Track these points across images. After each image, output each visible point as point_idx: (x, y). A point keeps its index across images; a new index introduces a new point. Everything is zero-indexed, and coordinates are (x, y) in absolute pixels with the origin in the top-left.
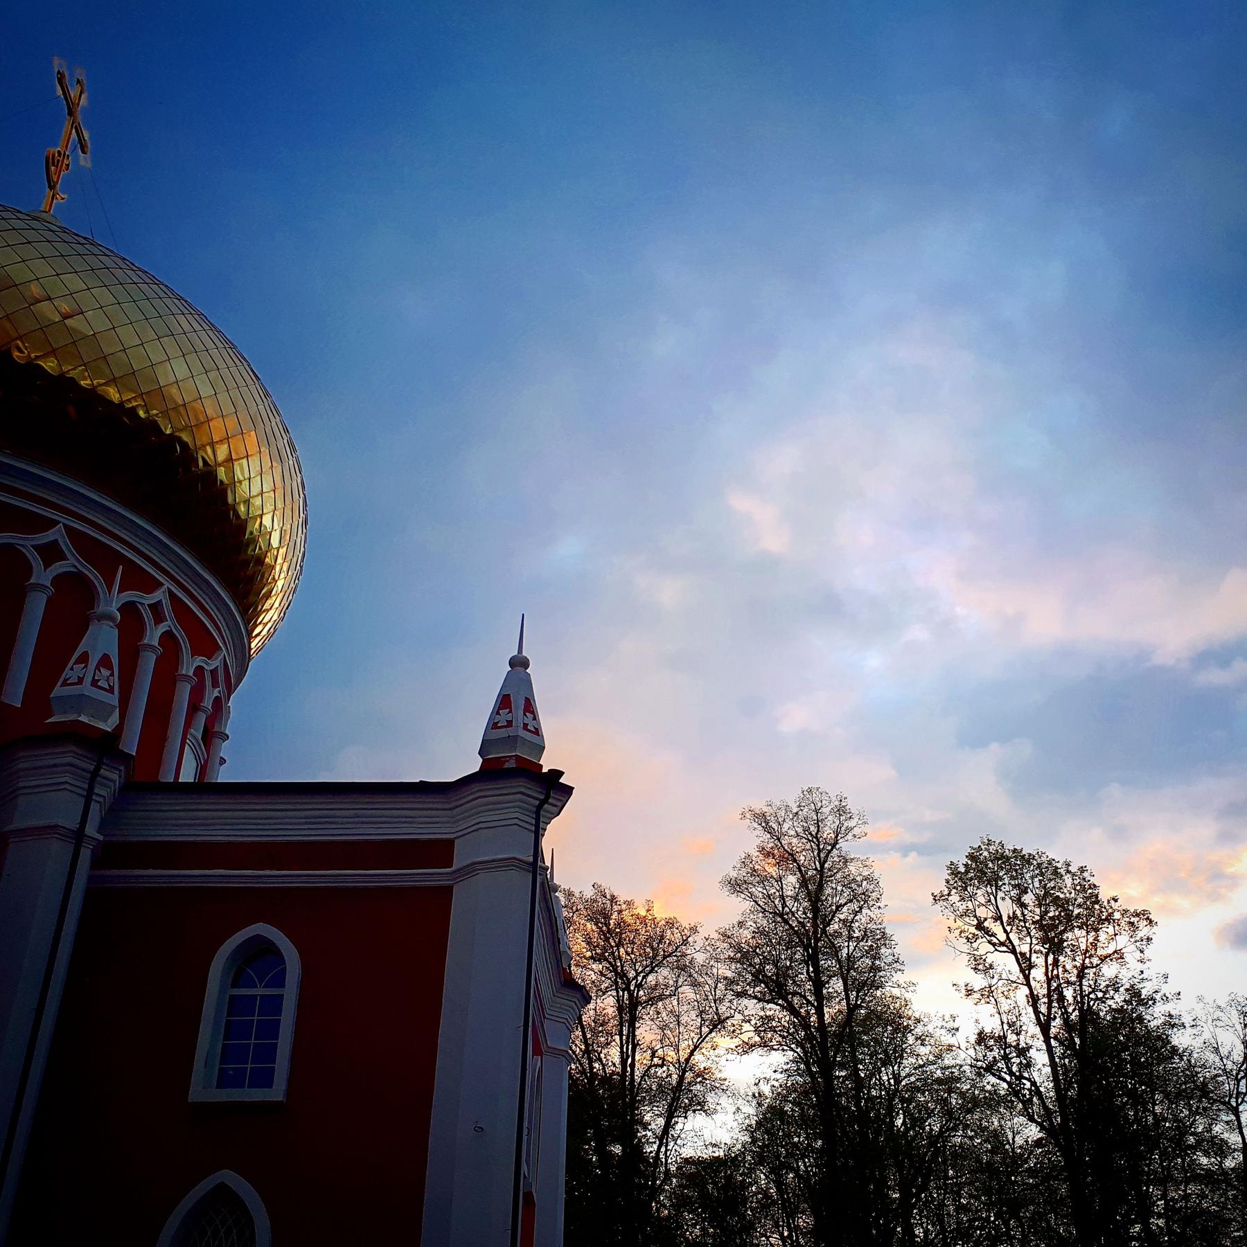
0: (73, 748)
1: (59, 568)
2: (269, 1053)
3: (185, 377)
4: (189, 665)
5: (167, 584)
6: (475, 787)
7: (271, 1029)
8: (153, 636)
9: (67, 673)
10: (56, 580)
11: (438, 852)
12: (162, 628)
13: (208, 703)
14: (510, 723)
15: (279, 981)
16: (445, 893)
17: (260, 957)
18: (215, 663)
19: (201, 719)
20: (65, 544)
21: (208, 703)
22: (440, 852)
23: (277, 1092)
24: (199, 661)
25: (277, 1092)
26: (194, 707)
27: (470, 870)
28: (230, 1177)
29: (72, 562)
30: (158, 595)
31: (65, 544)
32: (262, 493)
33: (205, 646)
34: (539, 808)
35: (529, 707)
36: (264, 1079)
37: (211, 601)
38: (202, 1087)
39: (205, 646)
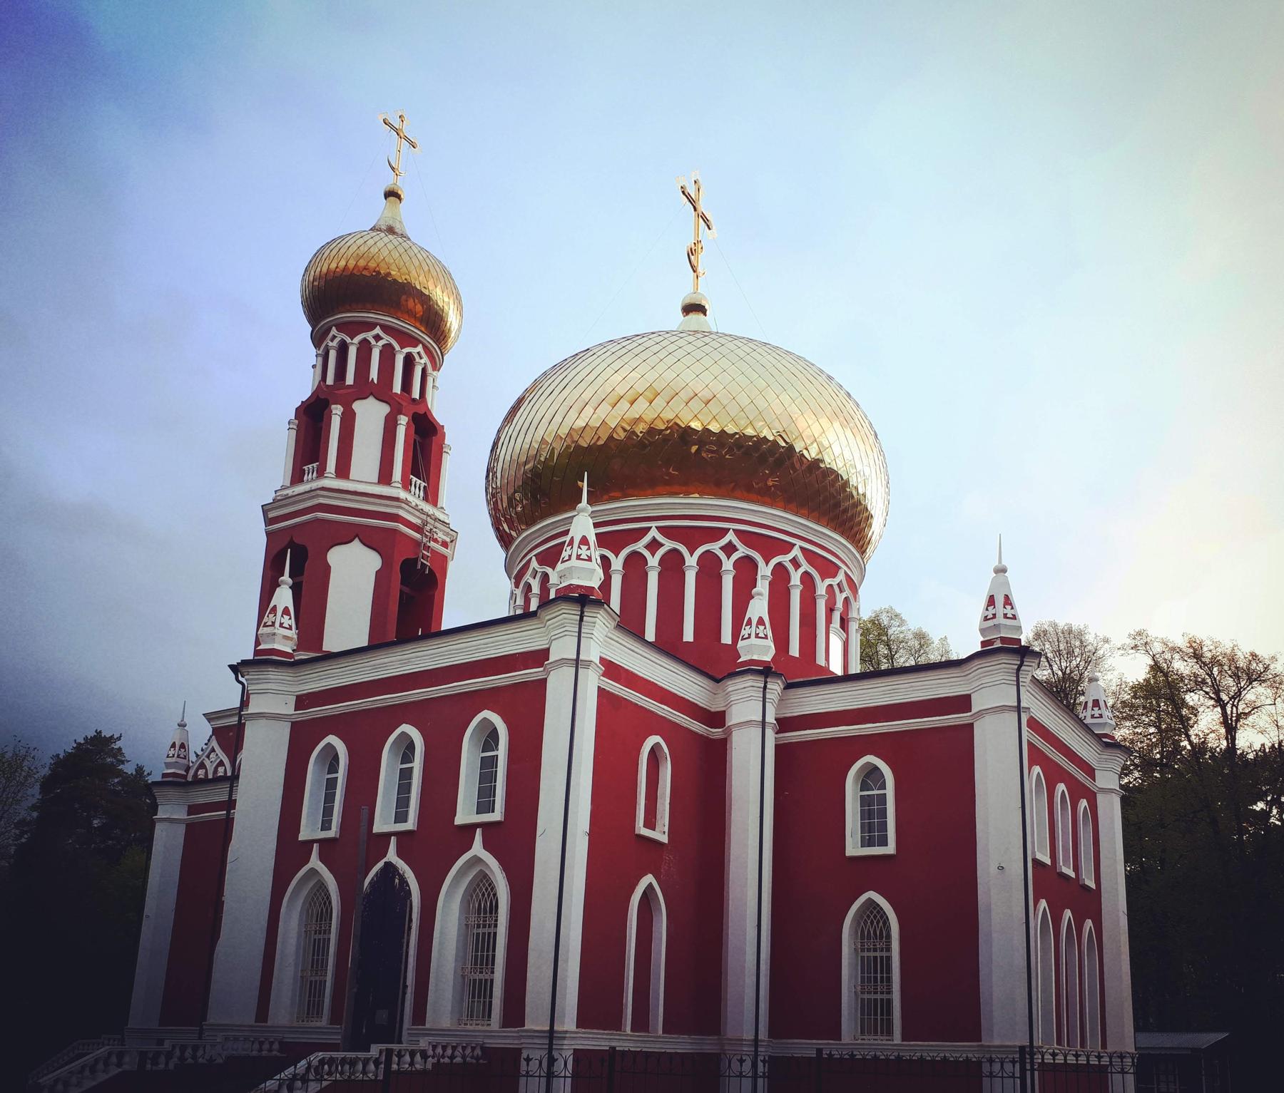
0: (750, 683)
1: (735, 556)
2: (883, 826)
3: (65, 745)
4: (821, 588)
5: (799, 543)
6: (976, 662)
7: (883, 813)
8: (796, 578)
9: (743, 632)
10: (736, 564)
11: (963, 703)
12: (801, 571)
13: (839, 605)
14: (994, 615)
15: (883, 787)
16: (970, 727)
17: (871, 775)
18: (841, 577)
19: (836, 617)
20: (736, 542)
21: (839, 605)
22: (963, 703)
23: (890, 849)
24: (828, 581)
25: (890, 849)
26: (830, 610)
27: (981, 713)
28: (872, 895)
29: (742, 550)
30: (796, 552)
31: (736, 542)
32: (577, 662)
33: (829, 569)
34: (1018, 670)
35: (1008, 601)
36: (884, 842)
37: (833, 542)
38: (853, 847)
39: (829, 569)
